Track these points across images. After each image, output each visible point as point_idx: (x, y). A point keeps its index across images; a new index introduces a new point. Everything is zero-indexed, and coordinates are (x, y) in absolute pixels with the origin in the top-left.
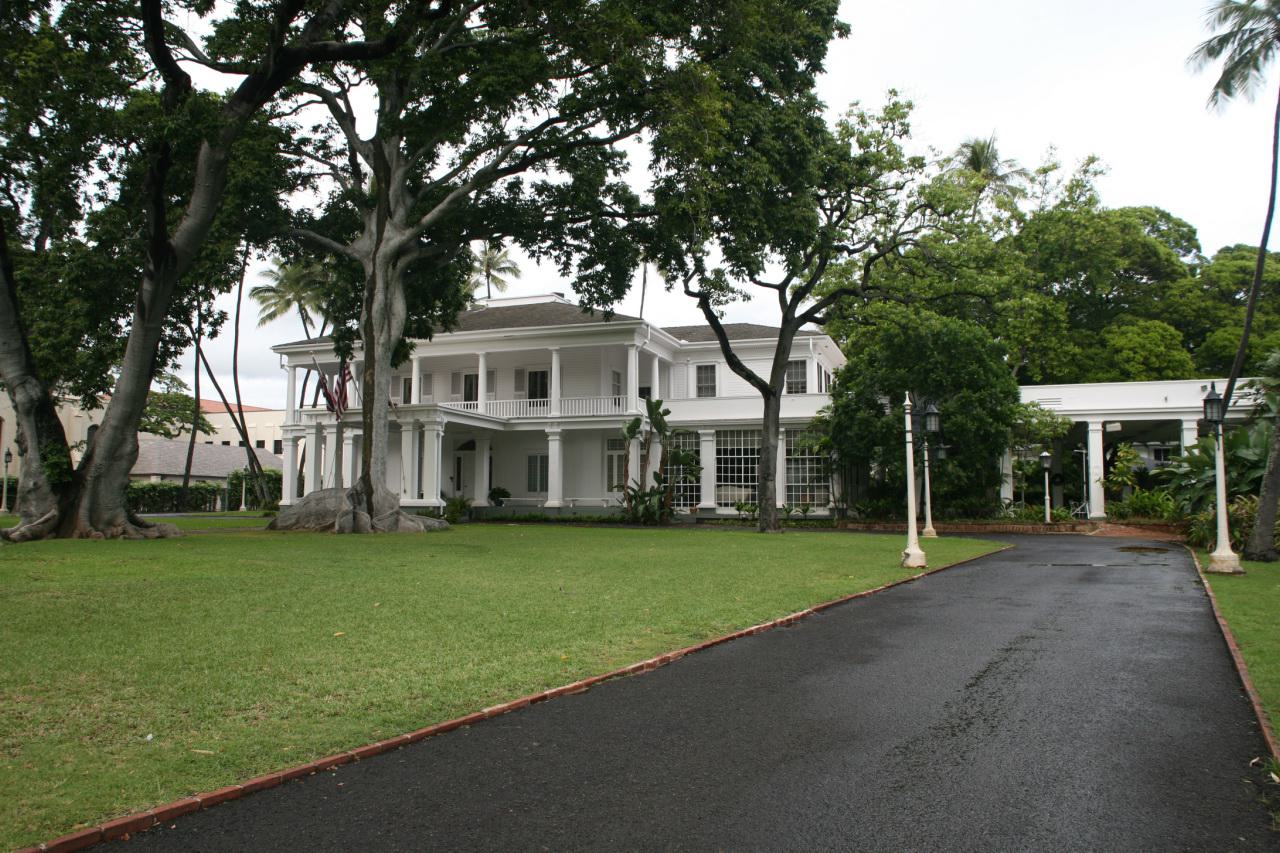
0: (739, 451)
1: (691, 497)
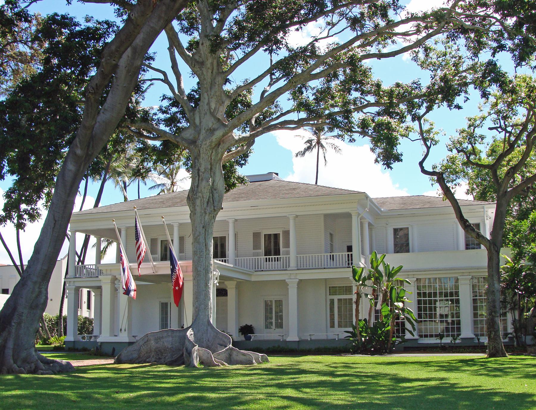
0: (435, 294)
1: (453, 329)
